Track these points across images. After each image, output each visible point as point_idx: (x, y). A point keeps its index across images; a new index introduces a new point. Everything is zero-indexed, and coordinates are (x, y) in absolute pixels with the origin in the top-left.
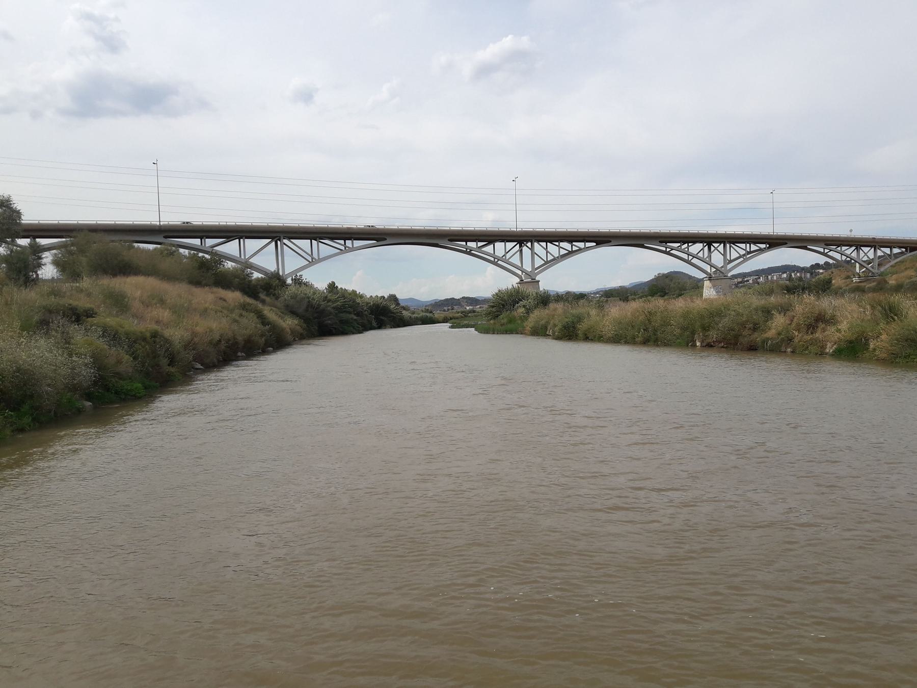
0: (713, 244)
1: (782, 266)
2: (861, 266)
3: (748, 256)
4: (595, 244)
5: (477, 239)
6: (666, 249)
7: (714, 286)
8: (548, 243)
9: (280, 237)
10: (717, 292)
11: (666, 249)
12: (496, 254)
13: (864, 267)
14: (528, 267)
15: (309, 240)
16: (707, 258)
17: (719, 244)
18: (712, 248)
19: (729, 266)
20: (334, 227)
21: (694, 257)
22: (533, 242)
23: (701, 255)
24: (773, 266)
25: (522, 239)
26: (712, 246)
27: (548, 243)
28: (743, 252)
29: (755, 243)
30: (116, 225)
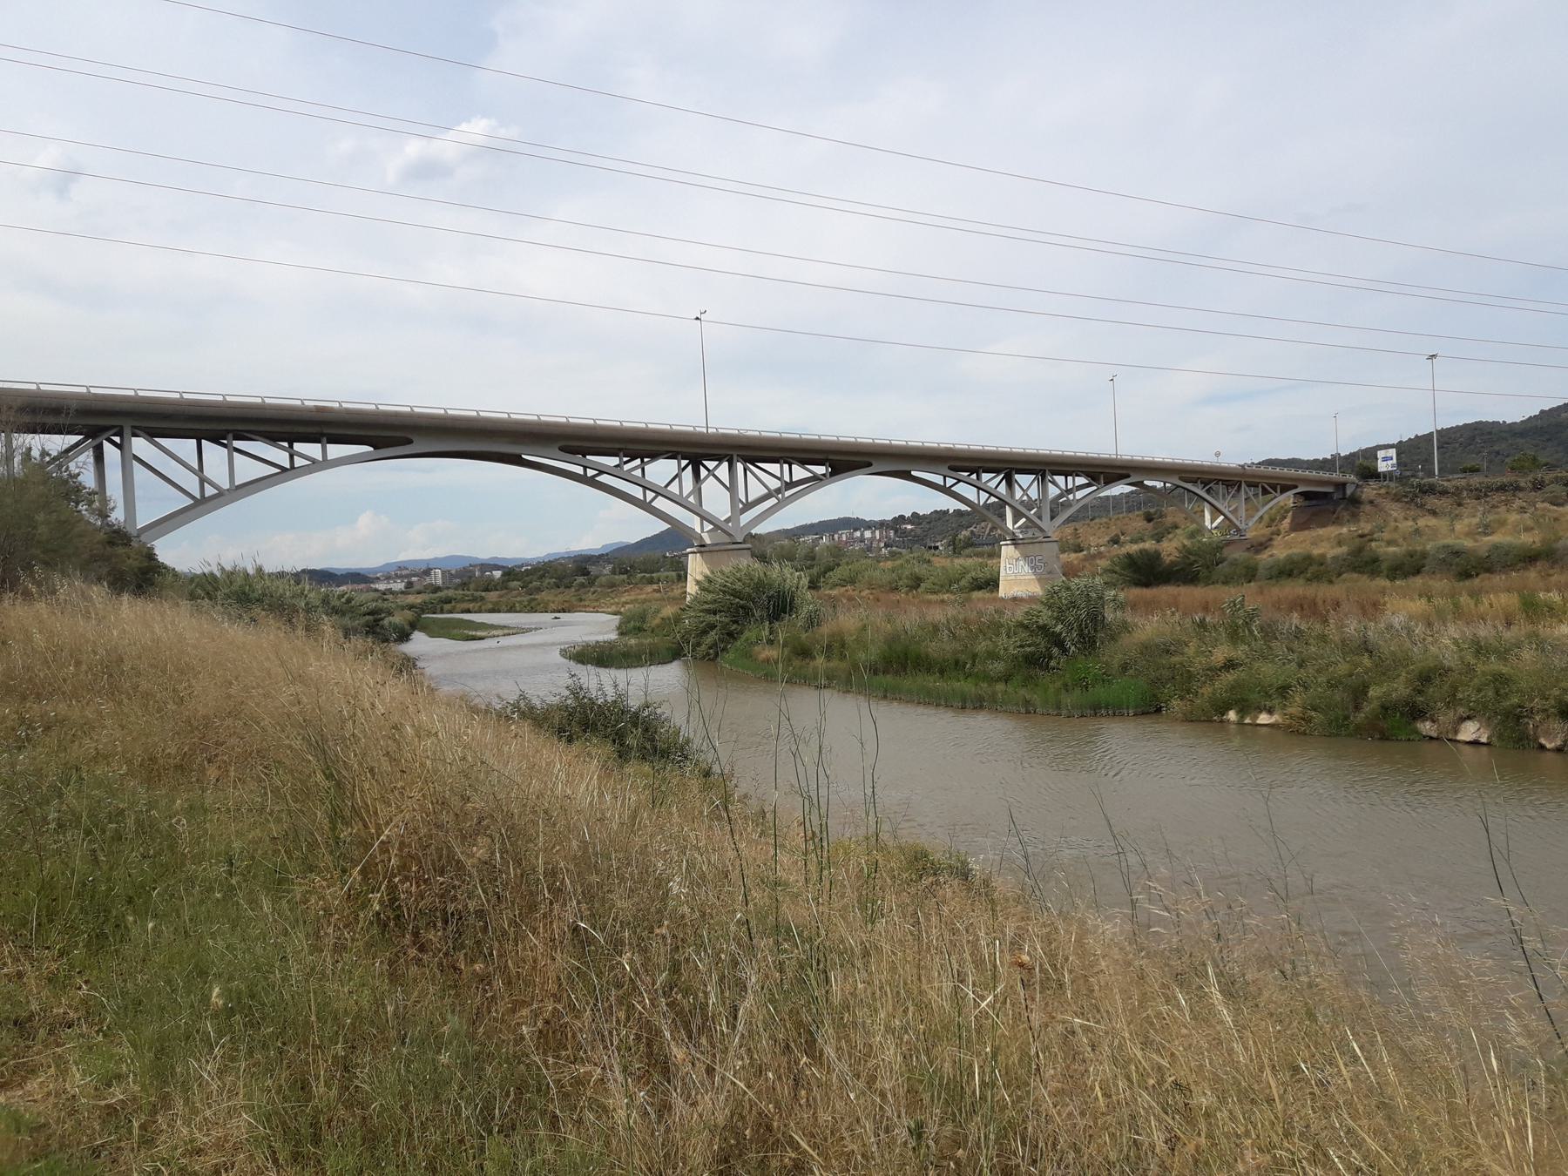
0: (704, 462)
2: (1017, 515)
3: (787, 494)
4: (368, 449)
5: (620, 450)
6: (585, 471)
7: (1026, 557)
9: (732, 455)
10: (1032, 568)
11: (585, 471)
13: (1024, 516)
16: (689, 496)
17: (717, 463)
18: (703, 472)
19: (745, 518)
20: (103, 395)
21: (658, 494)
22: (735, 461)
23: (674, 488)
24: (832, 518)
26: (701, 467)
28: (774, 484)
29: (803, 462)
30: (540, 424)
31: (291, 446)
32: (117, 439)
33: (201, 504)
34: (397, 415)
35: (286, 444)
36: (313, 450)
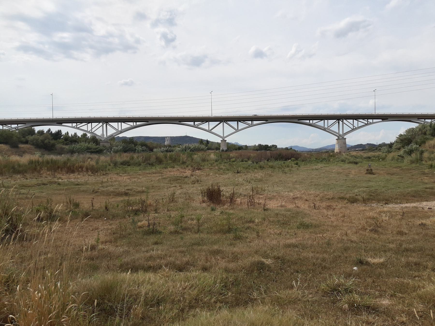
1: (139, 136)
4: (381, 120)
8: (354, 120)
12: (325, 127)
14: (341, 133)
15: (352, 120)
25: (339, 118)
27: (354, 120)
31: (368, 120)
32: (342, 120)
33: (353, 130)
34: (394, 115)
35: (367, 120)
36: (370, 121)
